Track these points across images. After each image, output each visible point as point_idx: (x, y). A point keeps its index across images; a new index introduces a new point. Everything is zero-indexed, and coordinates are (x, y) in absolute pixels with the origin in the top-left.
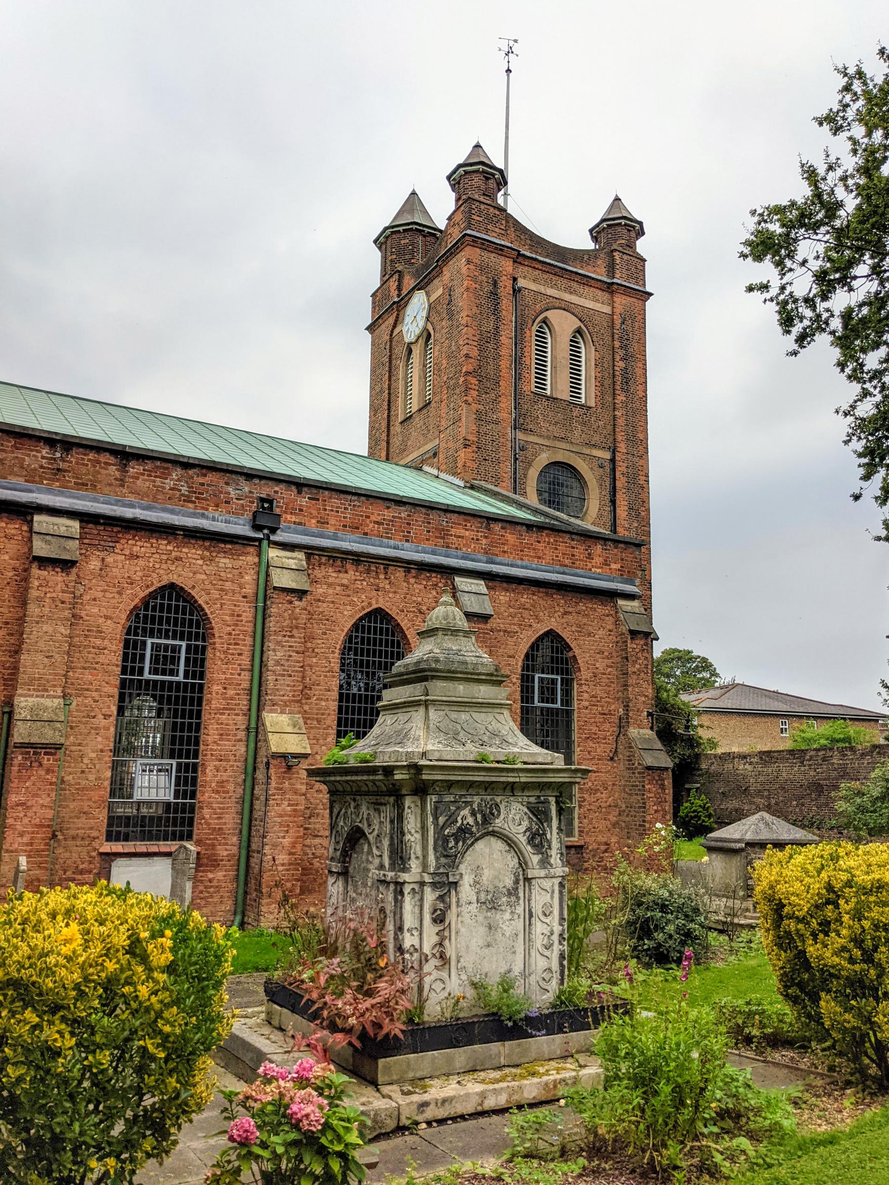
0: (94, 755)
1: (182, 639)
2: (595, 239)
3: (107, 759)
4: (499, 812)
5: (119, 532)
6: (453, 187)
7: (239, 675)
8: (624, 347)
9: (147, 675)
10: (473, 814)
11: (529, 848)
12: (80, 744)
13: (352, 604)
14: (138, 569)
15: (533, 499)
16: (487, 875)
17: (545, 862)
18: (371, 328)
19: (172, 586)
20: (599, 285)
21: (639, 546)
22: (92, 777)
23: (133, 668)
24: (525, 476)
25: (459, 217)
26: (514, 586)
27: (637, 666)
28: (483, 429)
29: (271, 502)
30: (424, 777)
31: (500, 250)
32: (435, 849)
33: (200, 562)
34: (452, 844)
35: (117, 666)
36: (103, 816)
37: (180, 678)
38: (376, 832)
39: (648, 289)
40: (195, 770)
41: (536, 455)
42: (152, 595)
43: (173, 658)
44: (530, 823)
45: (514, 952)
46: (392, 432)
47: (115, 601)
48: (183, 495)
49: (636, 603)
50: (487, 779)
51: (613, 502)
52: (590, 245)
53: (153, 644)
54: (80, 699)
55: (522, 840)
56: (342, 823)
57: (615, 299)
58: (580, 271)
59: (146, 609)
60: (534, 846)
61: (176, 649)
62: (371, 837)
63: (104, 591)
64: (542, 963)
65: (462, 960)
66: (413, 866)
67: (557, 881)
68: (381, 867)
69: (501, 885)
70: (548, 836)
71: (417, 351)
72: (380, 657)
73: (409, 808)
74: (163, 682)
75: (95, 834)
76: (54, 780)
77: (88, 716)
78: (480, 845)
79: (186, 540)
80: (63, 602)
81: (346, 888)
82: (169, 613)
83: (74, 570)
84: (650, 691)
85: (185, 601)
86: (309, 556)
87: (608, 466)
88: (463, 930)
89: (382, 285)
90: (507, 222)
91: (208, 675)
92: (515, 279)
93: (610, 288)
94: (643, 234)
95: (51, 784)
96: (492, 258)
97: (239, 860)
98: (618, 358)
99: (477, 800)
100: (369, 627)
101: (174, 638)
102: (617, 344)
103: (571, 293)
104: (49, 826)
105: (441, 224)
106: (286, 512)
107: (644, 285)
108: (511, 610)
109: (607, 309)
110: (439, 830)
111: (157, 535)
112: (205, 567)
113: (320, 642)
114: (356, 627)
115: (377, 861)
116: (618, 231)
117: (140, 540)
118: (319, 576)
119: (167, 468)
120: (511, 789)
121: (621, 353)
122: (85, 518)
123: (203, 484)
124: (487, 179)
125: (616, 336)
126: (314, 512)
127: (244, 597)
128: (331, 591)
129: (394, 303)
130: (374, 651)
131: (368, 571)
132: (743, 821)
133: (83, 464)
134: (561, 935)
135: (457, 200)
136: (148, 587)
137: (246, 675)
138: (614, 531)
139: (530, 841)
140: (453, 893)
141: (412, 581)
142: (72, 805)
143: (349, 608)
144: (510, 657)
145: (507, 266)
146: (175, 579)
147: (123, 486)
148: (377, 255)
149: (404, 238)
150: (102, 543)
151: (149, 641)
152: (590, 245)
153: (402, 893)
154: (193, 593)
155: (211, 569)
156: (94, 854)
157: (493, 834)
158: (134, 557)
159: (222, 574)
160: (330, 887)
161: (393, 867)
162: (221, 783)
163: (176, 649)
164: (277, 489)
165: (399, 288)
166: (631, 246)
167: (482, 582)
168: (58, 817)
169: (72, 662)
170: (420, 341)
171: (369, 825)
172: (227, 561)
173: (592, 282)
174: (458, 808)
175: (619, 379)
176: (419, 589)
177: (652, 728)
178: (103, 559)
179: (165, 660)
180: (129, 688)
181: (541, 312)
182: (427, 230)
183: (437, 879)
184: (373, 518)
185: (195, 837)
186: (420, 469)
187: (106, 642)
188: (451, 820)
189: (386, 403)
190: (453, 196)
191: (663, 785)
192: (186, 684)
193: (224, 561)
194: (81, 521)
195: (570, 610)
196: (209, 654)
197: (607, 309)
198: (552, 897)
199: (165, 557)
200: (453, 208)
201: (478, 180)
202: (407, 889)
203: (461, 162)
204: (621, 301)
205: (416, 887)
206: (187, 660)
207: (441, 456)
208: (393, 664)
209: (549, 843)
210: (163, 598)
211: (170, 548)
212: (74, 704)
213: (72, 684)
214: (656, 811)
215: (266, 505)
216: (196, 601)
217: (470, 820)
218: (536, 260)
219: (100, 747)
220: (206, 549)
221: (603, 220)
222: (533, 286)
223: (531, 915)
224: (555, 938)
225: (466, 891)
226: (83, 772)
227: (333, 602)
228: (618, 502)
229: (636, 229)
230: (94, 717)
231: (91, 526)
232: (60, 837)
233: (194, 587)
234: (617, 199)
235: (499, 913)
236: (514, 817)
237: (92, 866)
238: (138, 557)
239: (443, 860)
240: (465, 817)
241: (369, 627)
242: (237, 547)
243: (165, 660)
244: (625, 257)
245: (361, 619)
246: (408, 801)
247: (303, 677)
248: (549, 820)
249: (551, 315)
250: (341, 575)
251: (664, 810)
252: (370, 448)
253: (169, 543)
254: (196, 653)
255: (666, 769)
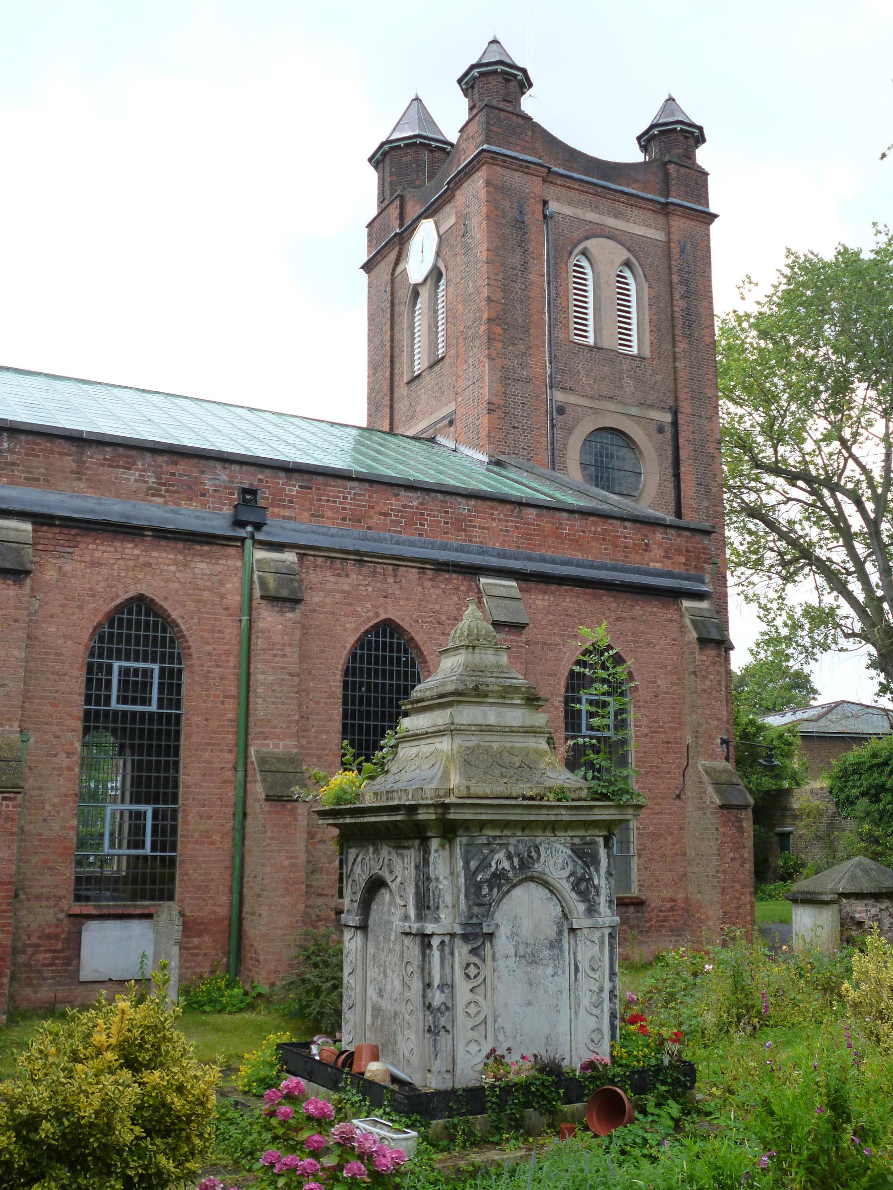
0: (56, 800)
1: (154, 661)
2: (644, 148)
3: (72, 804)
4: (539, 855)
5: (77, 535)
6: (466, 93)
7: (223, 703)
8: (685, 282)
9: (114, 705)
10: (509, 857)
11: (574, 895)
12: (40, 788)
13: (355, 614)
14: (99, 578)
15: (575, 473)
16: (526, 928)
17: (592, 911)
18: (367, 267)
19: (141, 599)
20: (650, 206)
21: (707, 533)
22: (56, 827)
23: (98, 697)
24: (565, 446)
25: (473, 129)
26: (553, 587)
27: (708, 683)
28: (511, 390)
29: (253, 492)
30: (451, 816)
31: (524, 167)
32: (466, 896)
33: (173, 568)
34: (485, 890)
35: (80, 694)
36: (69, 871)
37: (154, 708)
38: (399, 880)
39: (712, 209)
40: (174, 818)
41: (577, 421)
42: (119, 609)
43: (144, 684)
44: (575, 867)
45: (558, 1011)
46: (396, 395)
47: (76, 617)
48: (150, 488)
49: (704, 605)
50: (526, 818)
51: (677, 476)
52: (637, 156)
53: (120, 667)
54: (38, 735)
55: (565, 887)
56: (359, 871)
57: (672, 223)
58: (626, 189)
59: (111, 626)
60: (579, 893)
61: (147, 673)
62: (393, 886)
63: (63, 606)
64: (592, 1022)
65: (499, 1020)
66: (442, 916)
67: (607, 932)
68: (406, 918)
69: (542, 937)
70: (596, 882)
71: (424, 293)
72: (384, 678)
73: (436, 851)
74: (134, 713)
75: (61, 892)
76: (15, 829)
77: (49, 755)
78: (517, 892)
79: (156, 542)
80: (16, 621)
81: (365, 944)
82: (139, 627)
83: (28, 582)
84: (725, 713)
85: (156, 615)
86: (301, 556)
87: (668, 430)
88: (499, 986)
89: (379, 214)
90: (534, 132)
91: (185, 704)
92: (545, 203)
93: (665, 210)
94: (704, 141)
95: (12, 834)
96: (515, 178)
97: (230, 925)
98: (677, 296)
99: (512, 841)
100: (377, 642)
101: (145, 660)
102: (675, 278)
103: (616, 217)
104: (10, 883)
105: (452, 136)
106: (273, 505)
107: (707, 205)
108: (551, 617)
109: (660, 236)
110: (470, 876)
111: (122, 536)
112: (178, 574)
113: (317, 661)
114: (361, 643)
115: (399, 913)
116: (674, 141)
117: (102, 544)
118: (316, 581)
119: (132, 457)
120: (553, 827)
121: (681, 289)
122: (41, 520)
123: (173, 474)
124: (507, 81)
125: (674, 269)
126: (307, 504)
127: (226, 609)
128: (328, 600)
129: (396, 234)
130: (376, 670)
131: (374, 573)
132: (836, 868)
133: (34, 456)
134: (611, 992)
135: (471, 109)
136: (112, 599)
137: (230, 704)
138: (679, 514)
139: (575, 887)
140: (488, 945)
141: (428, 584)
142: (35, 859)
143: (351, 619)
144: (549, 675)
145: (533, 186)
146: (144, 589)
147: (80, 479)
148: (372, 176)
149: (406, 154)
150: (59, 548)
151: (116, 665)
152: (637, 156)
153: (430, 946)
154: (165, 605)
155: (184, 576)
156: (62, 916)
157: (532, 879)
158: (95, 564)
159: (199, 582)
160: (346, 944)
161: (420, 917)
162: (206, 834)
163: (147, 673)
164: (260, 477)
165: (402, 217)
166: (691, 157)
167: (514, 584)
168: (20, 874)
169: (28, 691)
170: (429, 282)
171: (391, 872)
172: (204, 566)
173: (643, 204)
174: (492, 851)
175: (679, 322)
176: (438, 592)
177: (727, 759)
178: (60, 568)
179: (134, 688)
180: (92, 721)
181: (580, 242)
182: (434, 144)
183: (470, 930)
184: (377, 509)
185: (177, 897)
186: (432, 440)
187: (67, 667)
188: (484, 865)
189: (388, 360)
190: (465, 102)
191: (741, 827)
192: (160, 714)
193: (201, 567)
194: (33, 523)
195: (624, 615)
196: (185, 679)
197: (660, 236)
198: (602, 950)
199: (131, 563)
200: (465, 117)
201: (496, 83)
202: (435, 941)
203: (474, 62)
204: (679, 225)
205: (447, 939)
206: (161, 685)
207: (459, 424)
208: (413, 687)
209: (597, 888)
210: (130, 612)
211: (136, 552)
212: (32, 740)
213: (29, 717)
214: (733, 859)
215: (248, 497)
216: (169, 616)
217: (506, 864)
218: (571, 178)
219: (64, 790)
220: (180, 552)
221: (652, 127)
222: (568, 210)
223: (577, 970)
224: (606, 995)
225: (503, 943)
226: (45, 820)
227: (332, 613)
228: (682, 476)
229: (694, 136)
230: (55, 756)
231: (45, 528)
232: (23, 896)
233: (166, 599)
234: (671, 99)
235: (541, 968)
236: (556, 859)
237: (59, 930)
238: (100, 564)
239: (476, 910)
240: (500, 860)
241: (377, 642)
242: (215, 547)
243: (134, 688)
244: (683, 170)
245: (367, 632)
246: (435, 844)
247: (300, 706)
248: (596, 862)
249: (592, 244)
250: (342, 579)
251: (742, 857)
252: (369, 415)
253: (136, 546)
254: (171, 677)
255: (745, 807)
